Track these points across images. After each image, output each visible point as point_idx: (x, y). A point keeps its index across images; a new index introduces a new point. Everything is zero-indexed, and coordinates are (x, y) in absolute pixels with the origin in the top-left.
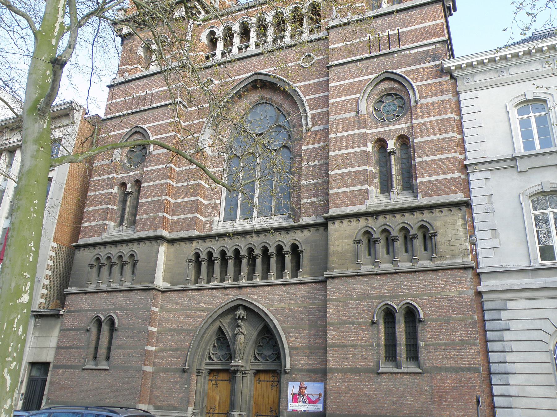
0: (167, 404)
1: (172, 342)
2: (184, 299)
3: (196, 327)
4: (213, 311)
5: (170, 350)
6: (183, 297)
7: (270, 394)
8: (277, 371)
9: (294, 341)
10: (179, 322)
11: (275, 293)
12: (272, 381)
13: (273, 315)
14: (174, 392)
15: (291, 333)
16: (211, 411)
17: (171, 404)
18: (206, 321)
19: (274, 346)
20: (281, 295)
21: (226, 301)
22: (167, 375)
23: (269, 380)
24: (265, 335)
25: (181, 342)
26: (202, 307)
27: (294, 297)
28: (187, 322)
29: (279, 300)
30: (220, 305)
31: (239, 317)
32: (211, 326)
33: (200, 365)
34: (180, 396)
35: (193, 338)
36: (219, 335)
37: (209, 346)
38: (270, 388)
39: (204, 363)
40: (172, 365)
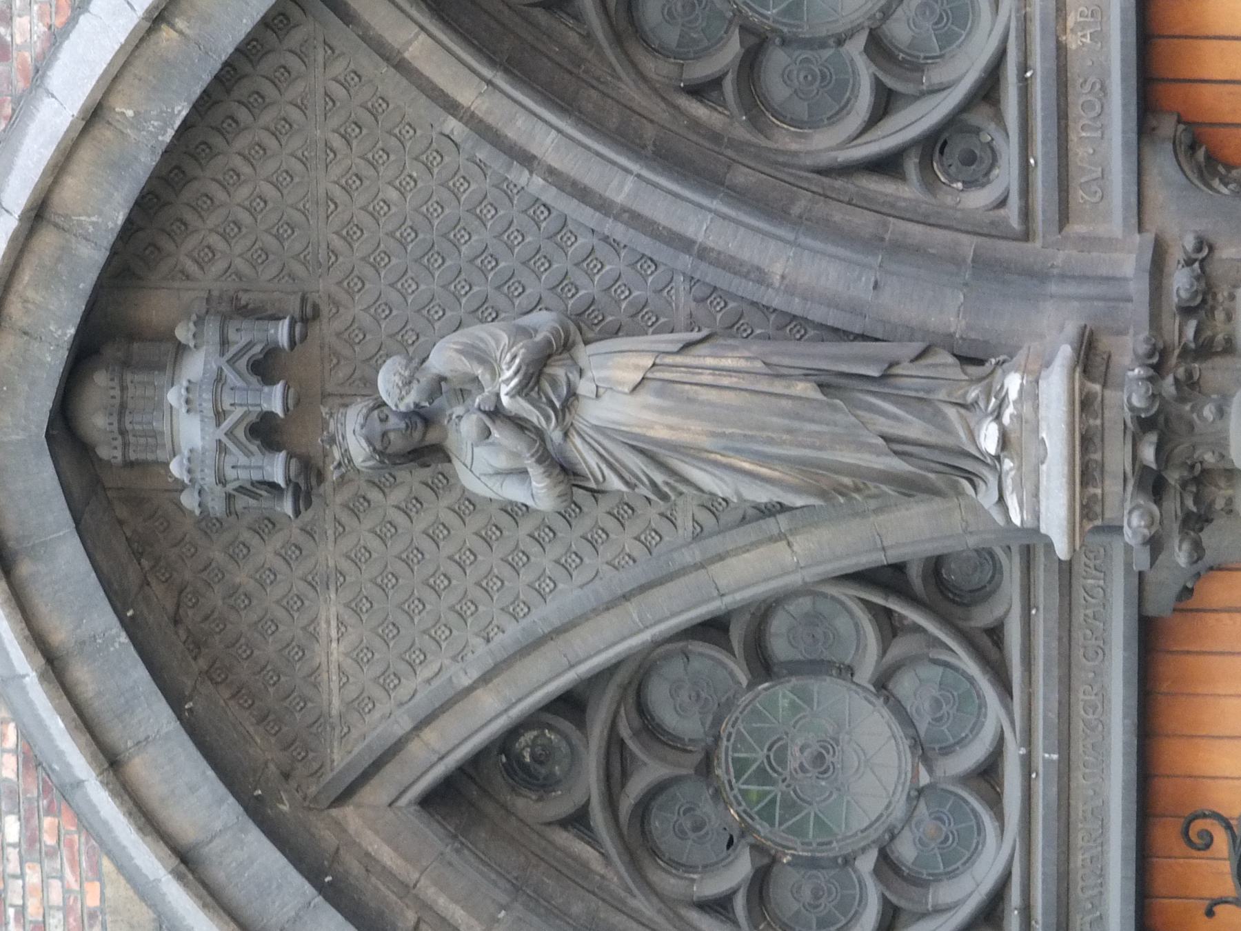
36: (578, 821)
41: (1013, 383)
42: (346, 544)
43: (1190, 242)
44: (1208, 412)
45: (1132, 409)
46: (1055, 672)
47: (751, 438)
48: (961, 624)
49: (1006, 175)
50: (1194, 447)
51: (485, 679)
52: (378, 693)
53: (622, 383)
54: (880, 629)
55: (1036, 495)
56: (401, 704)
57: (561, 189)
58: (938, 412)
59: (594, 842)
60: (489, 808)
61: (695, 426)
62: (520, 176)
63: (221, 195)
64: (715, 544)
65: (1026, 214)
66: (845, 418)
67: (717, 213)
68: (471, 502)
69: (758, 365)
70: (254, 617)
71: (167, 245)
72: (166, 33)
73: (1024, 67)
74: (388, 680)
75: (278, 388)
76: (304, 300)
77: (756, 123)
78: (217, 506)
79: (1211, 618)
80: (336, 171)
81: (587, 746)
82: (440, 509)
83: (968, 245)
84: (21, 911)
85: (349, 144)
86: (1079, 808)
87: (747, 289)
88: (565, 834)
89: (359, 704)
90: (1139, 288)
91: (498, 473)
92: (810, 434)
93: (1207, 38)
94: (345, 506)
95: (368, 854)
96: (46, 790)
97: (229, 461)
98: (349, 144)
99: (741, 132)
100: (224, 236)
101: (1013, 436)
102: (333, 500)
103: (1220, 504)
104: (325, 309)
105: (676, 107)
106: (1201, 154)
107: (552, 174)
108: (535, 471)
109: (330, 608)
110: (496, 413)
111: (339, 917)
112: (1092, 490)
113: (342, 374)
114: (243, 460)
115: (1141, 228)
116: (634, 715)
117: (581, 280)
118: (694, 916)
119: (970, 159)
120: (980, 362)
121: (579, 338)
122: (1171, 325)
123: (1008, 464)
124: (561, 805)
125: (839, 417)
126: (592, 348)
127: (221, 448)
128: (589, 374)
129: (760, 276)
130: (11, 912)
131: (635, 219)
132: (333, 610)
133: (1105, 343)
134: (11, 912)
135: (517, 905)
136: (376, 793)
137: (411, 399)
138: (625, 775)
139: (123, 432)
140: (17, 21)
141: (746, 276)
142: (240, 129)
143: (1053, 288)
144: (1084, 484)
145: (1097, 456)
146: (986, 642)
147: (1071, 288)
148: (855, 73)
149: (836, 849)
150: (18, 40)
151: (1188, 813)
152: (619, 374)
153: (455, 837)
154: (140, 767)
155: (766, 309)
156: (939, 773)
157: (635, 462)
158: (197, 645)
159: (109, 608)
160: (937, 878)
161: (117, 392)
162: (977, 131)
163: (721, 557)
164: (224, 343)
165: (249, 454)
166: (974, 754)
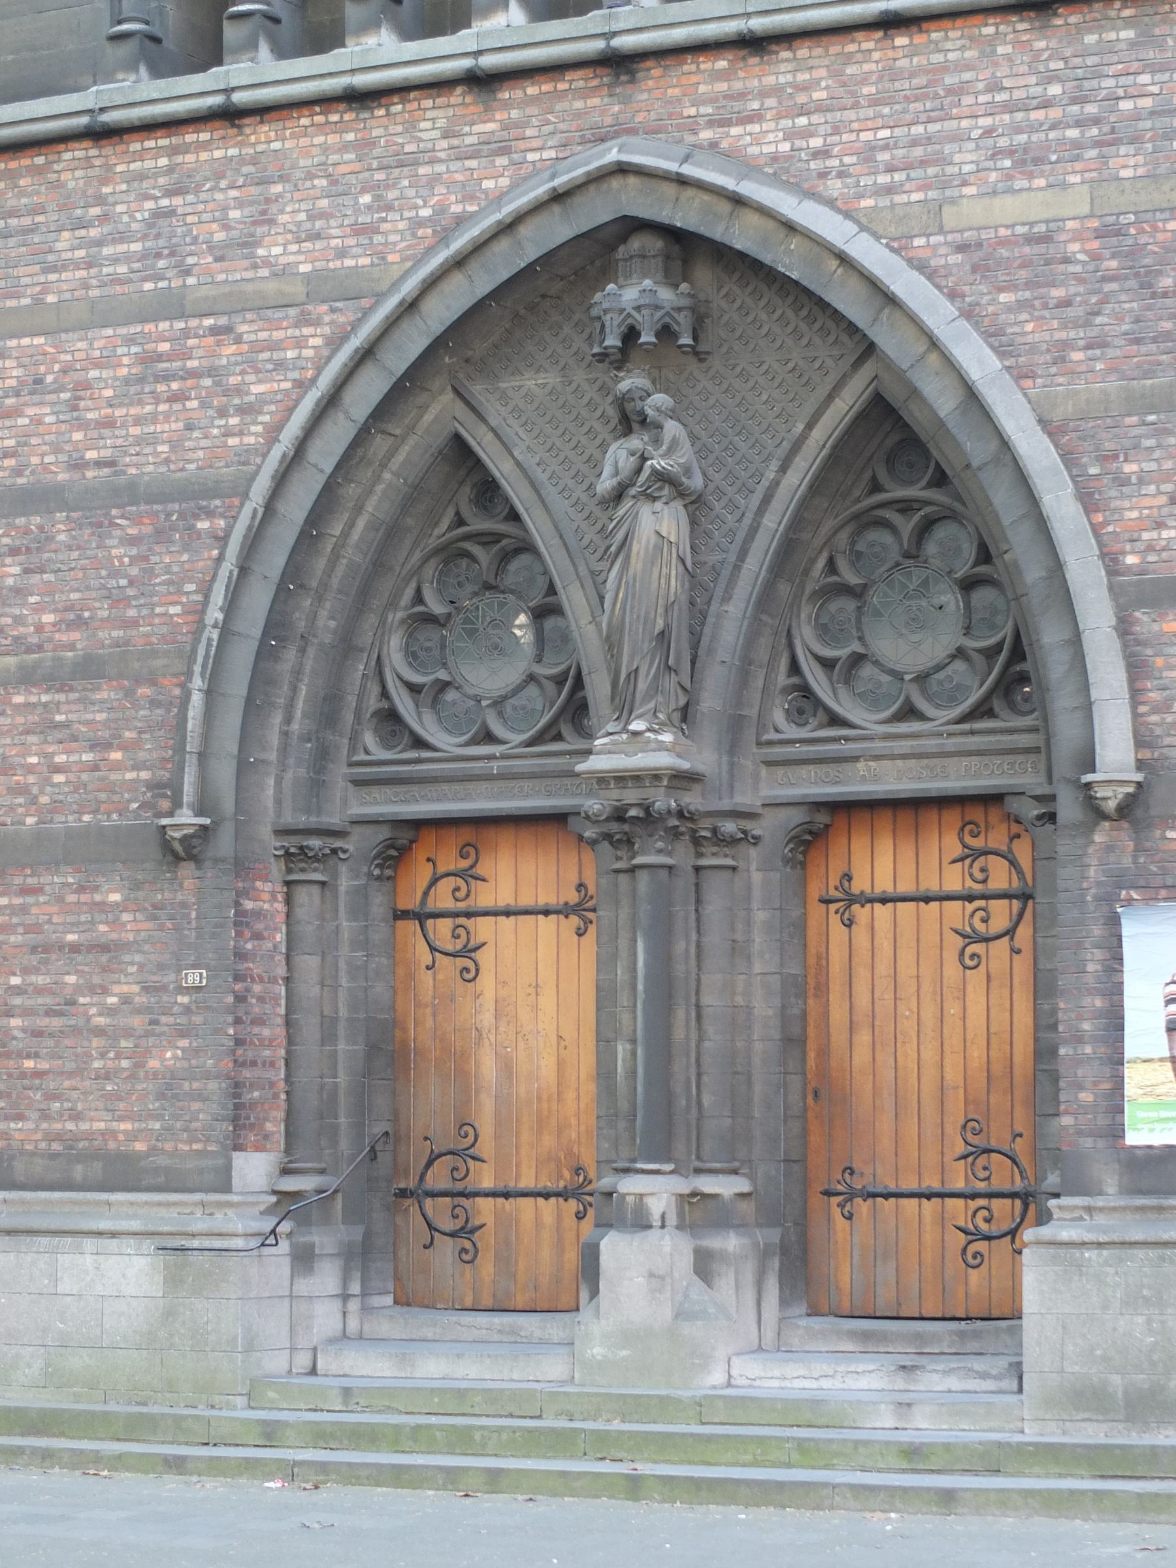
0: (50, 1137)
1: (39, 609)
2: (104, 218)
3: (244, 456)
4: (380, 297)
5: (27, 678)
6: (100, 200)
7: (953, 1009)
8: (1014, 805)
9: (1160, 525)
10: (83, 425)
11: (957, 91)
12: (970, 898)
13: (953, 295)
14: (100, 1032)
15: (1132, 450)
16: (438, 1178)
17: (89, 1136)
18: (331, 401)
19: (968, 585)
20: (1010, 107)
21: (499, 198)
22: (25, 891)
23: (931, 884)
24: (876, 487)
25: (118, 600)
26: (283, 273)
27: (1136, 116)
28: (154, 418)
29: (996, 154)
30: (444, 238)
31: (631, 335)
32: (379, 445)
33: (316, 786)
34: (153, 1063)
35: (220, 559)
36: (460, 521)
37: (372, 620)
38: (951, 956)
39: (339, 772)
40: (57, 806)
41: (667, 737)
42: (585, 386)
43: (756, 832)
44: (660, 844)
45: (654, 802)
46: (536, 770)
47: (633, 597)
48: (562, 719)
49: (792, 732)
50: (640, 837)
51: (518, 464)
52: (510, 408)
53: (660, 525)
54: (559, 675)
55: (610, 752)
56: (505, 420)
57: (768, 488)
58: (652, 698)
59: (450, 529)
60: (463, 472)
61: (639, 567)
62: (774, 465)
63: (762, 303)
64: (589, 583)
65: (770, 743)
66: (646, 647)
67: (759, 573)
68: (604, 447)
69: (672, 599)
70: (547, 338)
71: (736, 277)
72: (834, 263)
73: (847, 739)
74: (517, 411)
75: (654, 340)
76: (708, 353)
77: (815, 595)
78: (595, 312)
79: (575, 854)
80: (776, 366)
81: (497, 522)
82: (604, 433)
83: (753, 712)
84: (384, 220)
85: (790, 372)
86: (471, 786)
87: (719, 592)
88: (452, 514)
89: (504, 398)
90: (725, 805)
91: (616, 462)
92: (637, 628)
93: (895, 845)
94: (604, 383)
95: (428, 407)
96: (445, 230)
97: (615, 316)
98: (790, 372)
99: (810, 588)
100: (740, 308)
101: (639, 738)
102: (602, 373)
103: (619, 853)
104: (704, 365)
105: (820, 552)
106: (808, 837)
107: (776, 483)
108: (615, 481)
109: (552, 379)
110: (644, 458)
111: (386, 390)
112: (612, 782)
113: (672, 377)
114: (615, 323)
115: (764, 805)
116: (512, 547)
117: (723, 503)
118: (413, 585)
119: (801, 712)
120: (684, 719)
121: (687, 502)
122: (707, 823)
123: (625, 736)
124: (467, 511)
125: (646, 644)
126: (681, 509)
127: (622, 310)
128: (666, 507)
129: (726, 599)
130: (384, 215)
131: (754, 530)
132: (551, 380)
133: (697, 787)
134: (384, 215)
135: (406, 489)
136: (460, 409)
137: (650, 412)
138: (485, 544)
139: (631, 257)
140: (839, 181)
141: (726, 591)
142: (796, 312)
143: (725, 758)
144: (615, 778)
145: (630, 784)
146: (554, 732)
147: (725, 768)
148: (843, 648)
149: (451, 659)
150: (829, 183)
151: (479, 846)
152: (665, 523)
153: (440, 453)
154: (457, 280)
155: (709, 603)
156: (487, 711)
157: (620, 536)
158: (532, 308)
159: (537, 256)
160: (438, 713)
161: (652, 253)
162: (815, 716)
163: (582, 586)
164: (679, 309)
165: (619, 326)
166: (498, 729)
